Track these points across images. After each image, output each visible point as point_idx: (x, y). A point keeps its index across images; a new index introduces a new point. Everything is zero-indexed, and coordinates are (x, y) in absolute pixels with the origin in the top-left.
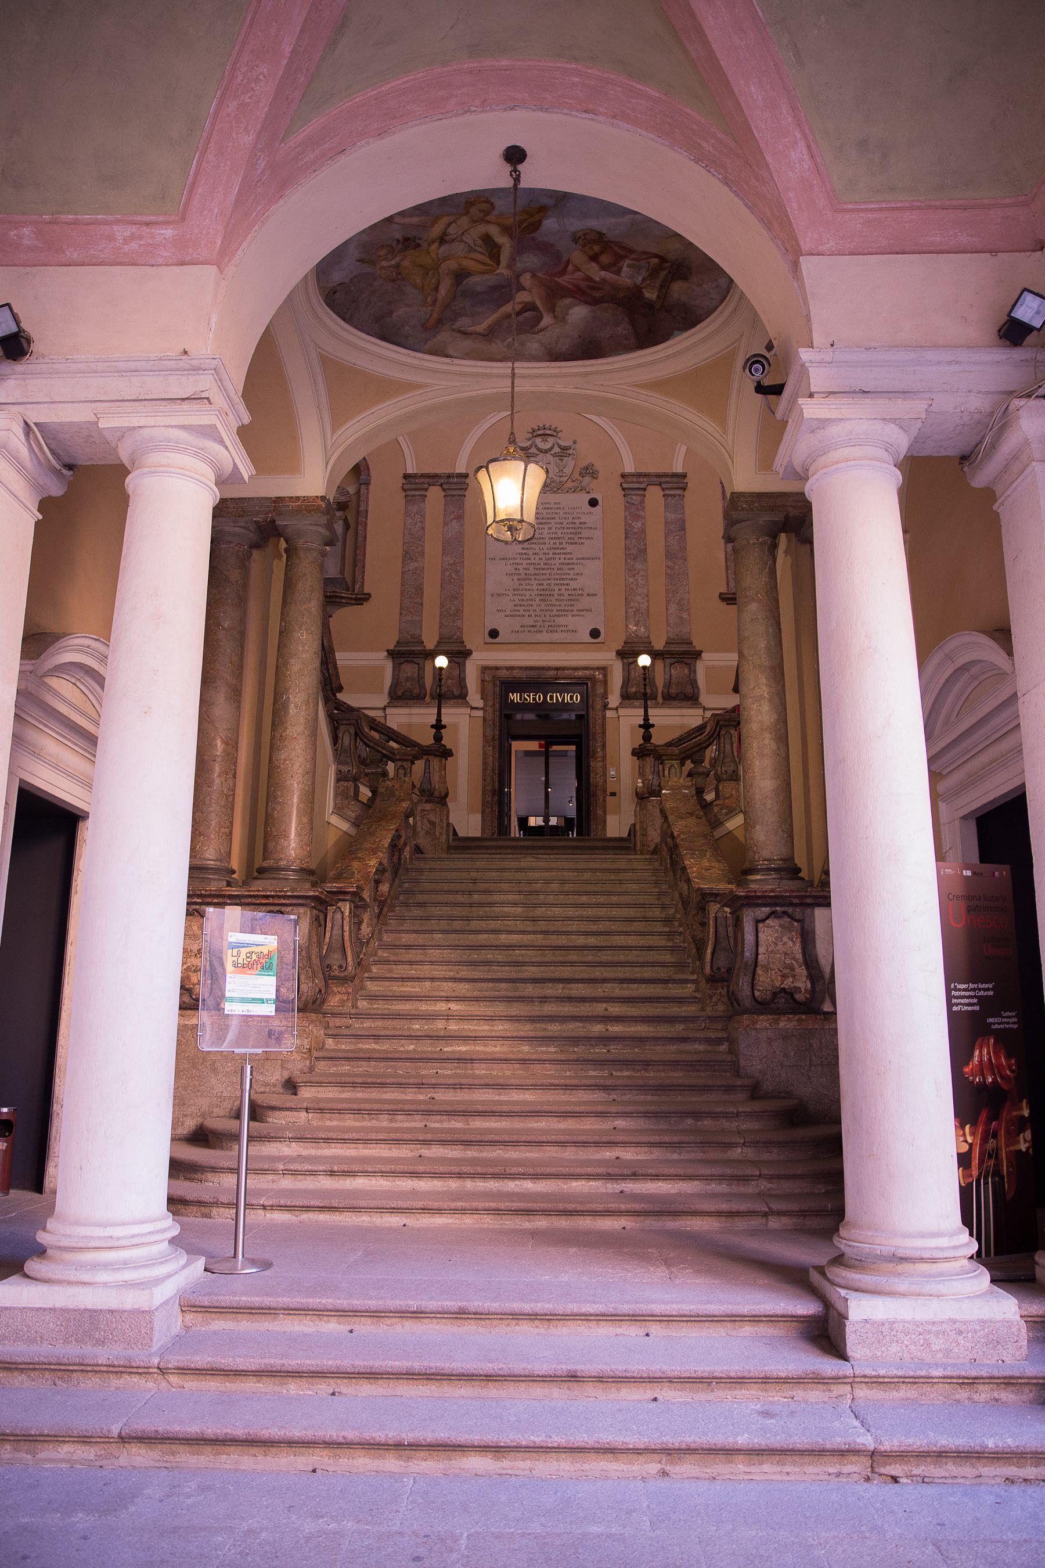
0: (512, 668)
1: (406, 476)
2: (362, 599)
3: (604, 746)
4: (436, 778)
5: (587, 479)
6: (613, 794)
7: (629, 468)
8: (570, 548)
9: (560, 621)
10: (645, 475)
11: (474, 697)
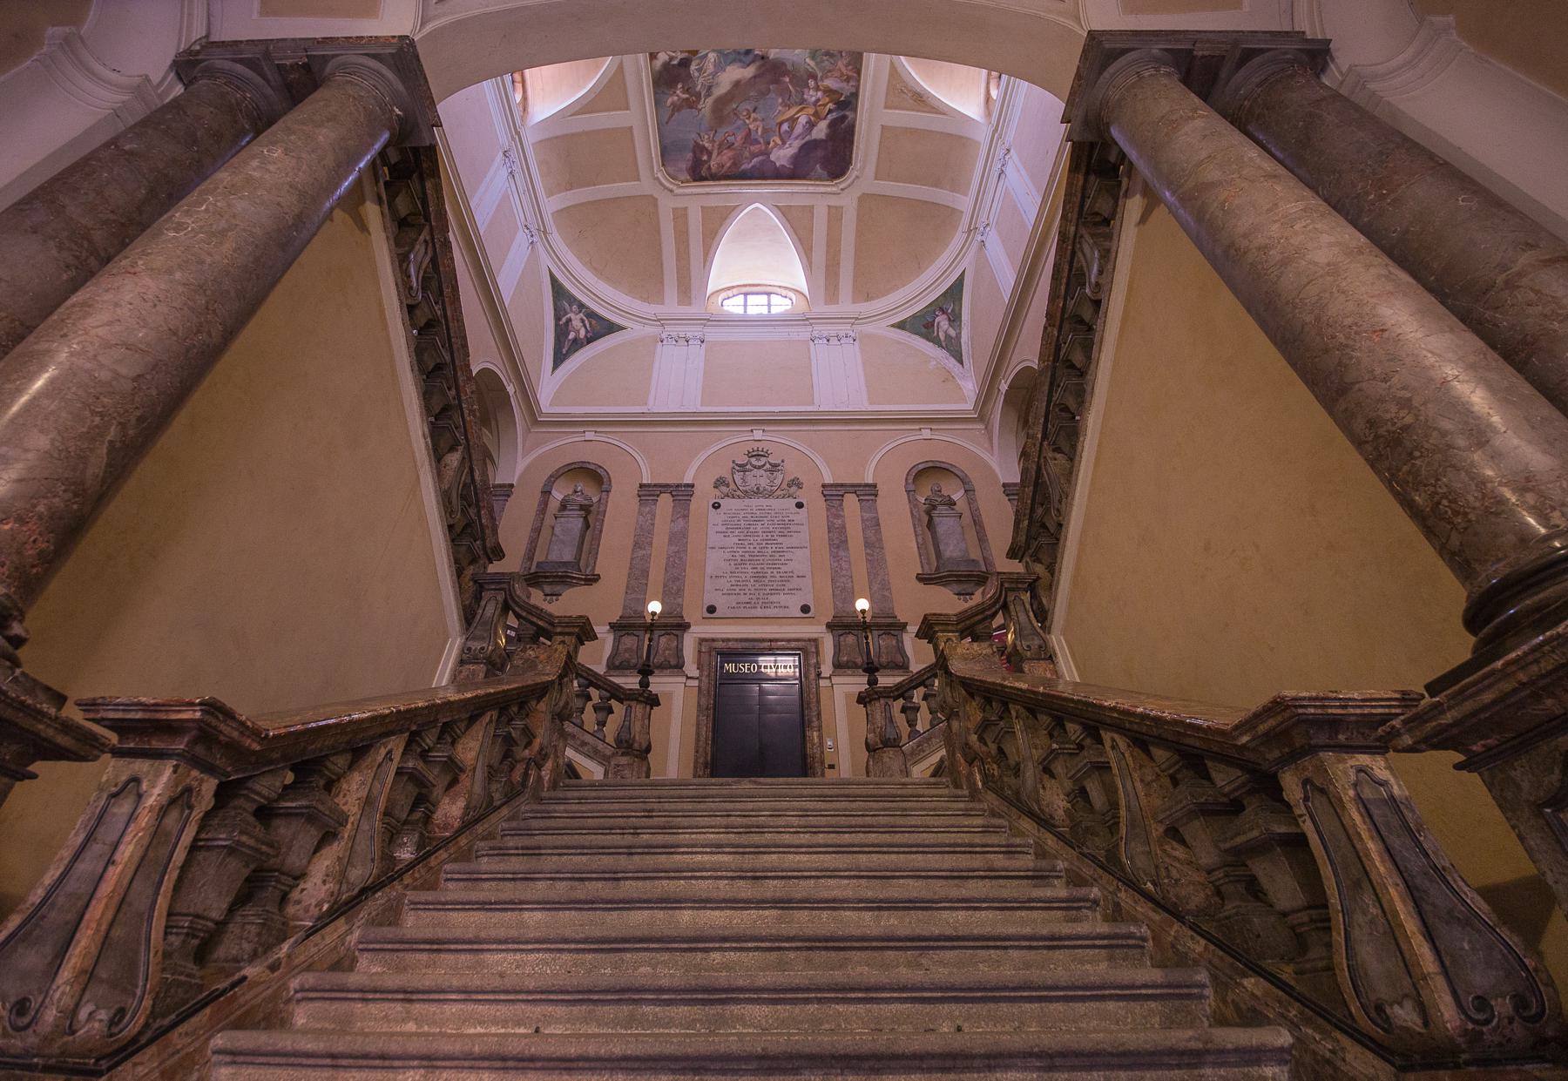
0: (729, 640)
1: (641, 486)
2: (592, 579)
3: (819, 714)
4: (637, 727)
5: (794, 488)
6: (832, 767)
7: (828, 480)
8: (780, 540)
9: (772, 598)
10: (842, 485)
11: (691, 668)
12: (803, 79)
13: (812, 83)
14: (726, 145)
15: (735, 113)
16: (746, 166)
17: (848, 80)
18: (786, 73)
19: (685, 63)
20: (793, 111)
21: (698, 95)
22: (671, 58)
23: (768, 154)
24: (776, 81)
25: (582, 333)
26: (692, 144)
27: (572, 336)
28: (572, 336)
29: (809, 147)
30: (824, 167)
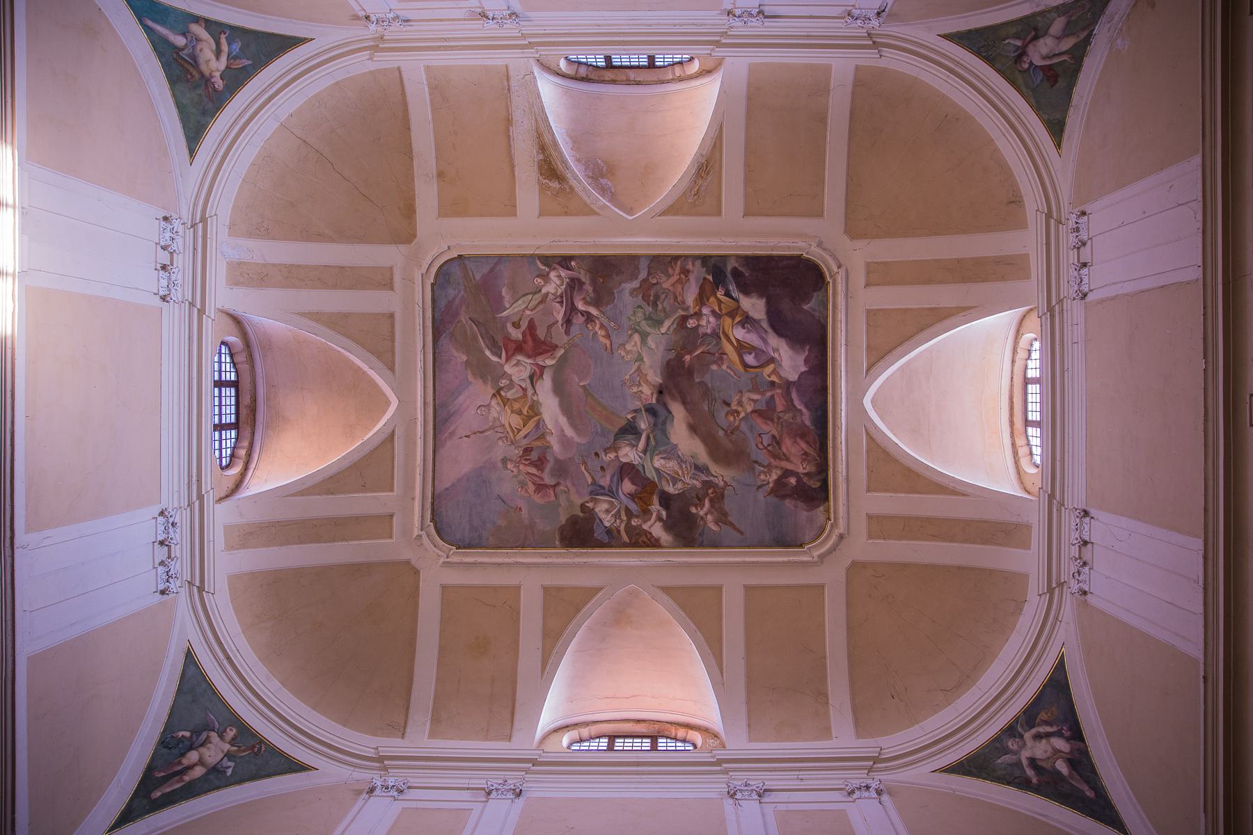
12: (687, 337)
13: (691, 323)
14: (776, 453)
15: (732, 431)
16: (807, 418)
17: (686, 272)
18: (679, 358)
19: (666, 500)
20: (729, 349)
21: (707, 485)
22: (659, 519)
23: (788, 385)
24: (690, 372)
25: (1060, 744)
26: (772, 499)
27: (1062, 767)
28: (1062, 767)
29: (779, 323)
30: (807, 298)
